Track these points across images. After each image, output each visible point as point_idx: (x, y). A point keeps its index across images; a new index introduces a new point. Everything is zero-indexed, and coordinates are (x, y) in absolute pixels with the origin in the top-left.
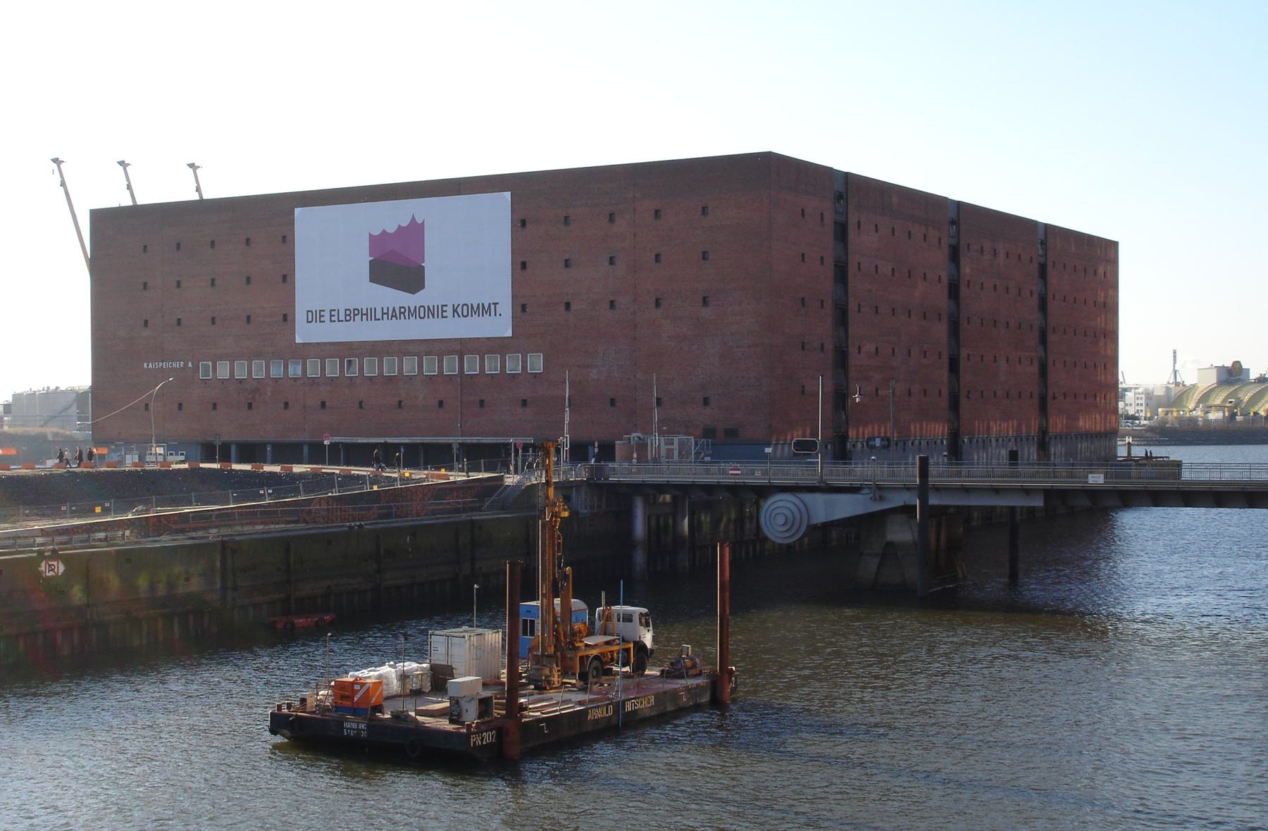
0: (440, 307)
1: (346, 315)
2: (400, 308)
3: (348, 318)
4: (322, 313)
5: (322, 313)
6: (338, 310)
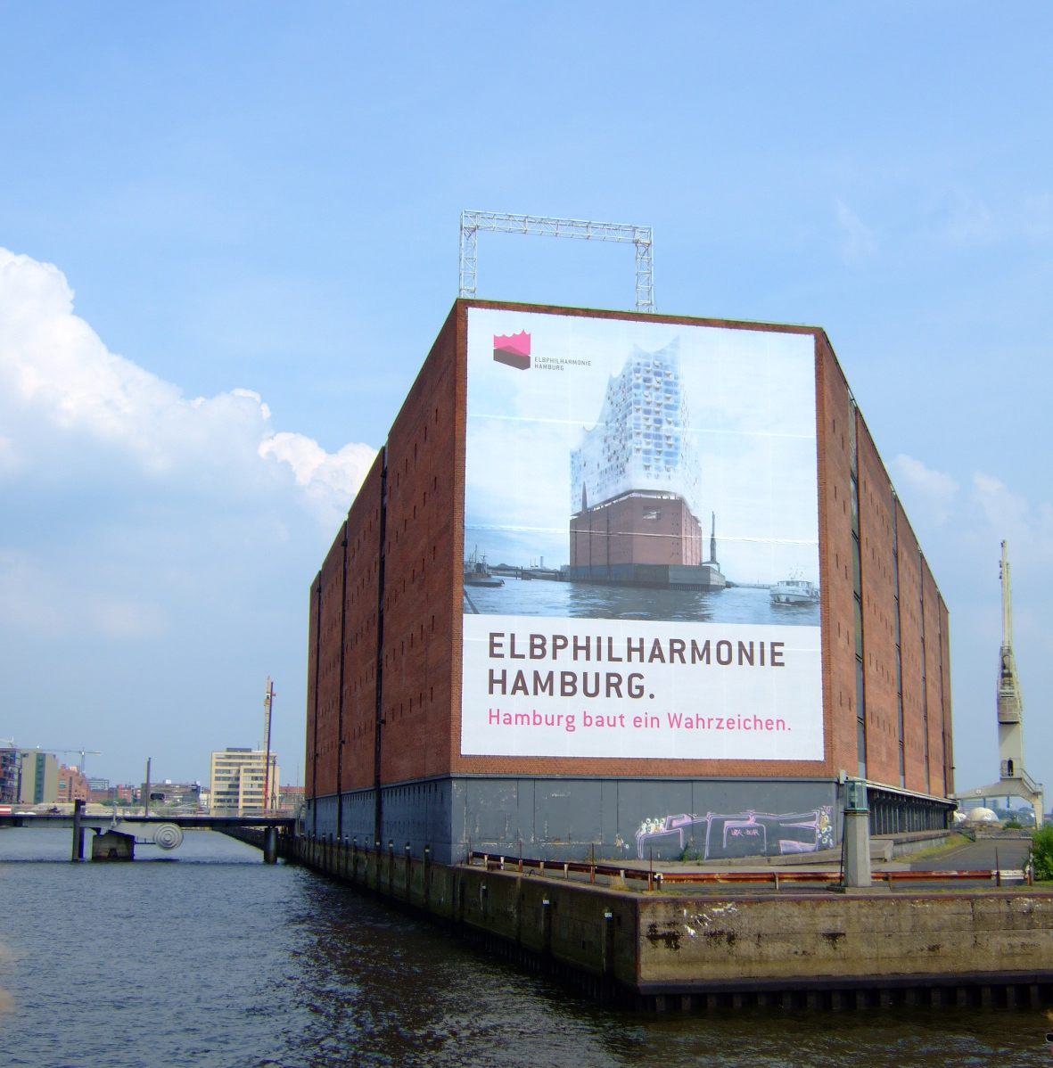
0: (767, 649)
1: (533, 646)
2: (672, 642)
3: (538, 652)
4: (777, 649)
5: (777, 649)
6: (513, 636)
